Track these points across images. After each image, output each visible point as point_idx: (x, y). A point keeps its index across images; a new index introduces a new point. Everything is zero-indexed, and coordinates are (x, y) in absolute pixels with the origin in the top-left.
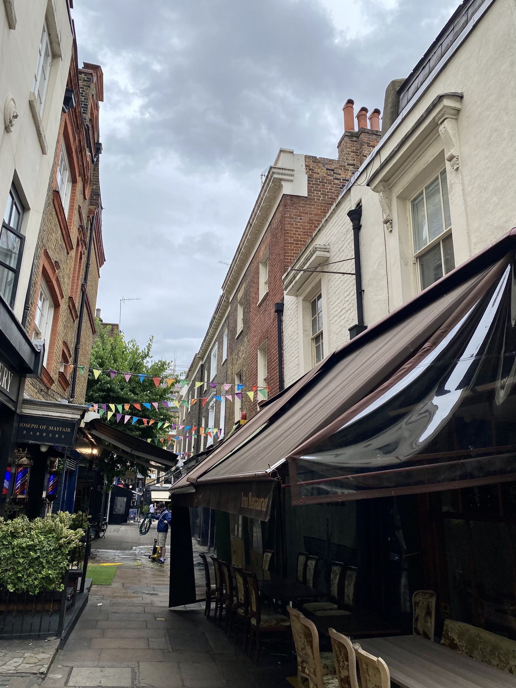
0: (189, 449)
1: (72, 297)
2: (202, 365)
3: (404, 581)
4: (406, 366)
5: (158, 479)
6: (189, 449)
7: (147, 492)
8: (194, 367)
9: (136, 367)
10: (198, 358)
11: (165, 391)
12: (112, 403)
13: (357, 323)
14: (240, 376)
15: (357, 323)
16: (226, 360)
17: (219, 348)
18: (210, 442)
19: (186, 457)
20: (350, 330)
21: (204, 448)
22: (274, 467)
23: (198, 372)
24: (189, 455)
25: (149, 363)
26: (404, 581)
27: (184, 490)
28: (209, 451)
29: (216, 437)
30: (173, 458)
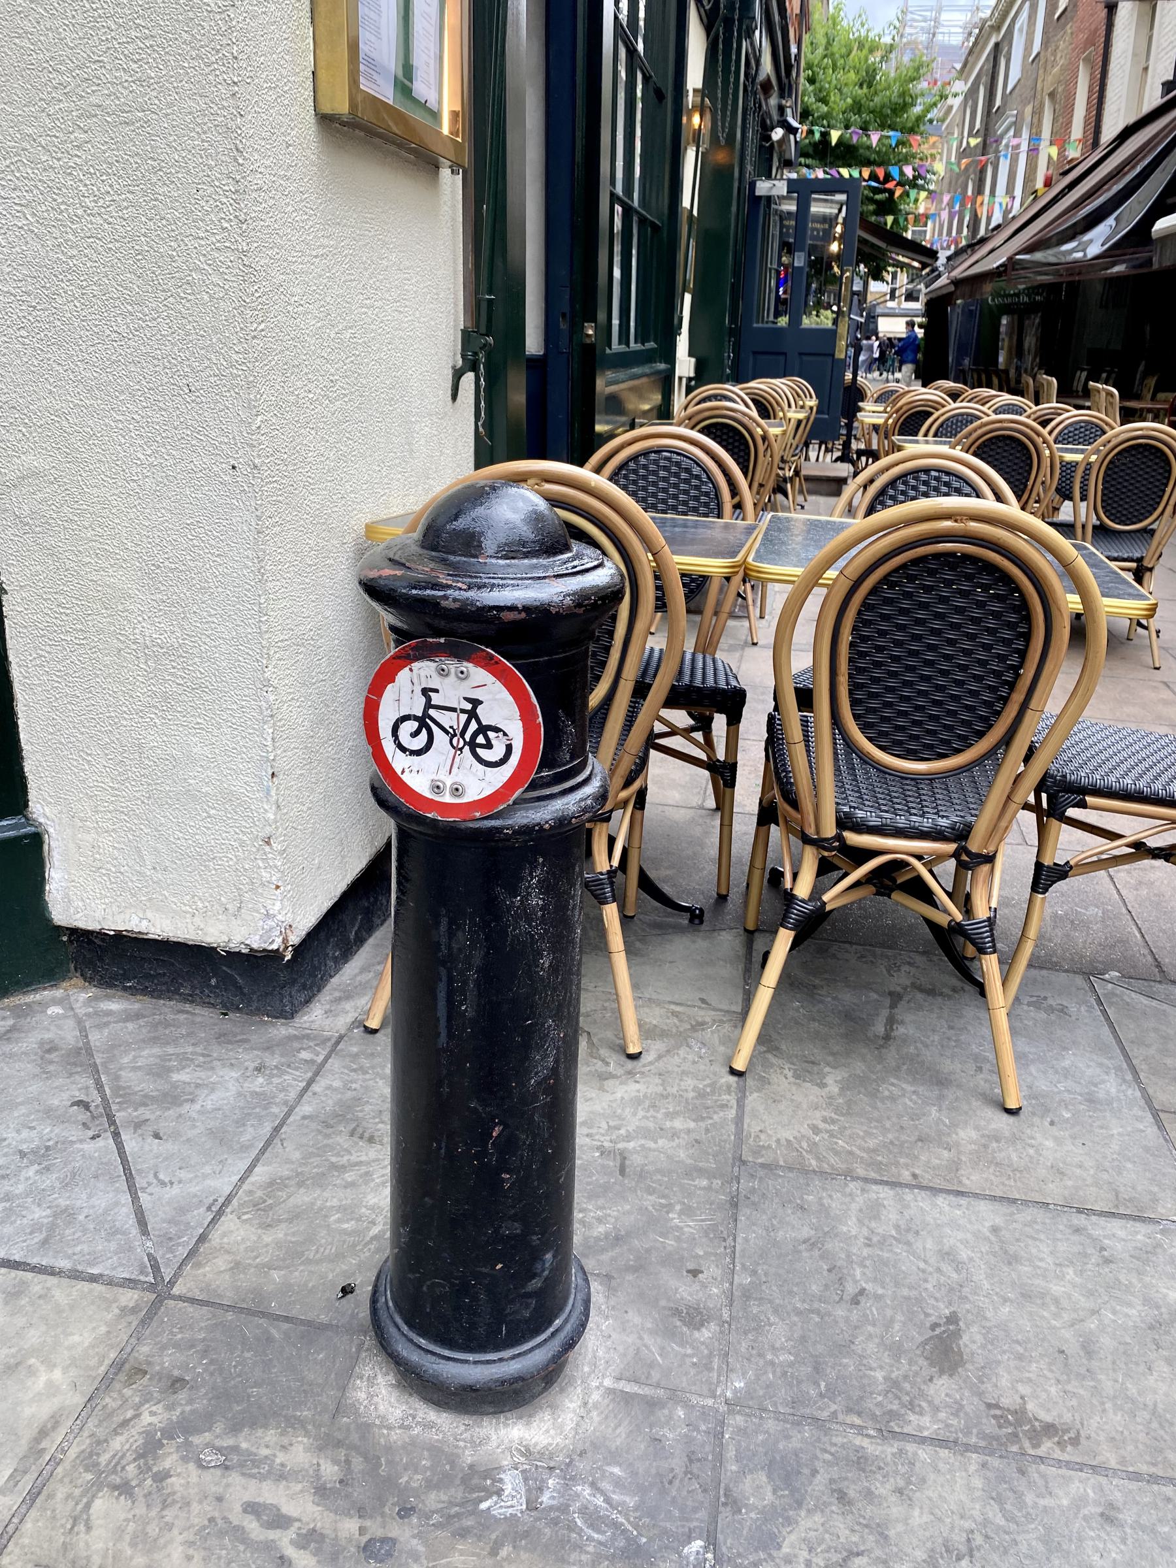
0: (959, 231)
1: (1058, 490)
2: (997, 45)
3: (1141, 368)
4: (1105, 187)
5: (893, 291)
6: (959, 231)
7: (872, 318)
8: (979, 47)
9: (868, 79)
10: (985, 30)
11: (919, 119)
12: (843, 166)
13: (1171, 78)
14: (1052, 95)
15: (1171, 78)
16: (1038, 55)
17: (1030, 17)
18: (997, 219)
19: (953, 247)
20: (1163, 84)
21: (987, 229)
22: (998, 263)
23: (987, 59)
24: (957, 244)
25: (889, 71)
26: (1141, 368)
27: (944, 291)
28: (983, 241)
29: (1006, 212)
30: (932, 254)
